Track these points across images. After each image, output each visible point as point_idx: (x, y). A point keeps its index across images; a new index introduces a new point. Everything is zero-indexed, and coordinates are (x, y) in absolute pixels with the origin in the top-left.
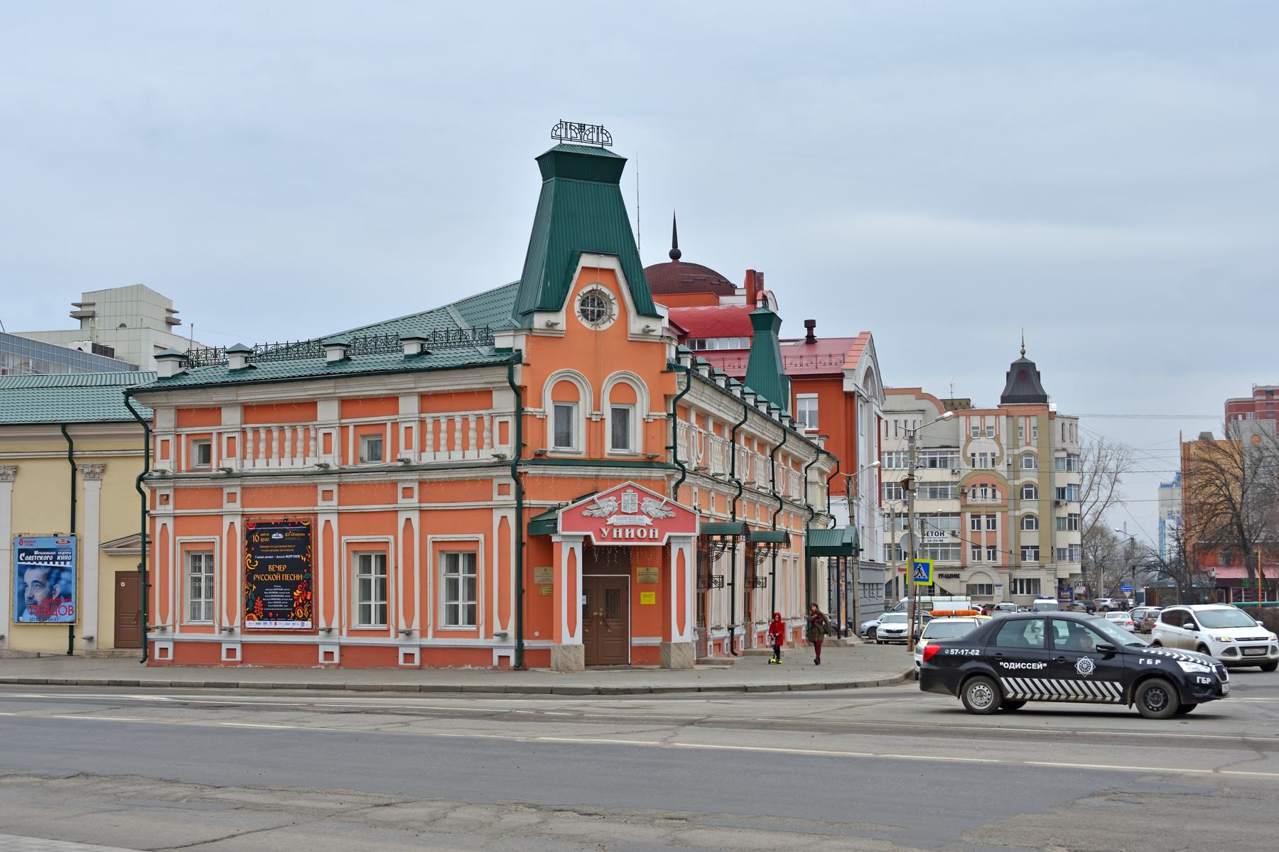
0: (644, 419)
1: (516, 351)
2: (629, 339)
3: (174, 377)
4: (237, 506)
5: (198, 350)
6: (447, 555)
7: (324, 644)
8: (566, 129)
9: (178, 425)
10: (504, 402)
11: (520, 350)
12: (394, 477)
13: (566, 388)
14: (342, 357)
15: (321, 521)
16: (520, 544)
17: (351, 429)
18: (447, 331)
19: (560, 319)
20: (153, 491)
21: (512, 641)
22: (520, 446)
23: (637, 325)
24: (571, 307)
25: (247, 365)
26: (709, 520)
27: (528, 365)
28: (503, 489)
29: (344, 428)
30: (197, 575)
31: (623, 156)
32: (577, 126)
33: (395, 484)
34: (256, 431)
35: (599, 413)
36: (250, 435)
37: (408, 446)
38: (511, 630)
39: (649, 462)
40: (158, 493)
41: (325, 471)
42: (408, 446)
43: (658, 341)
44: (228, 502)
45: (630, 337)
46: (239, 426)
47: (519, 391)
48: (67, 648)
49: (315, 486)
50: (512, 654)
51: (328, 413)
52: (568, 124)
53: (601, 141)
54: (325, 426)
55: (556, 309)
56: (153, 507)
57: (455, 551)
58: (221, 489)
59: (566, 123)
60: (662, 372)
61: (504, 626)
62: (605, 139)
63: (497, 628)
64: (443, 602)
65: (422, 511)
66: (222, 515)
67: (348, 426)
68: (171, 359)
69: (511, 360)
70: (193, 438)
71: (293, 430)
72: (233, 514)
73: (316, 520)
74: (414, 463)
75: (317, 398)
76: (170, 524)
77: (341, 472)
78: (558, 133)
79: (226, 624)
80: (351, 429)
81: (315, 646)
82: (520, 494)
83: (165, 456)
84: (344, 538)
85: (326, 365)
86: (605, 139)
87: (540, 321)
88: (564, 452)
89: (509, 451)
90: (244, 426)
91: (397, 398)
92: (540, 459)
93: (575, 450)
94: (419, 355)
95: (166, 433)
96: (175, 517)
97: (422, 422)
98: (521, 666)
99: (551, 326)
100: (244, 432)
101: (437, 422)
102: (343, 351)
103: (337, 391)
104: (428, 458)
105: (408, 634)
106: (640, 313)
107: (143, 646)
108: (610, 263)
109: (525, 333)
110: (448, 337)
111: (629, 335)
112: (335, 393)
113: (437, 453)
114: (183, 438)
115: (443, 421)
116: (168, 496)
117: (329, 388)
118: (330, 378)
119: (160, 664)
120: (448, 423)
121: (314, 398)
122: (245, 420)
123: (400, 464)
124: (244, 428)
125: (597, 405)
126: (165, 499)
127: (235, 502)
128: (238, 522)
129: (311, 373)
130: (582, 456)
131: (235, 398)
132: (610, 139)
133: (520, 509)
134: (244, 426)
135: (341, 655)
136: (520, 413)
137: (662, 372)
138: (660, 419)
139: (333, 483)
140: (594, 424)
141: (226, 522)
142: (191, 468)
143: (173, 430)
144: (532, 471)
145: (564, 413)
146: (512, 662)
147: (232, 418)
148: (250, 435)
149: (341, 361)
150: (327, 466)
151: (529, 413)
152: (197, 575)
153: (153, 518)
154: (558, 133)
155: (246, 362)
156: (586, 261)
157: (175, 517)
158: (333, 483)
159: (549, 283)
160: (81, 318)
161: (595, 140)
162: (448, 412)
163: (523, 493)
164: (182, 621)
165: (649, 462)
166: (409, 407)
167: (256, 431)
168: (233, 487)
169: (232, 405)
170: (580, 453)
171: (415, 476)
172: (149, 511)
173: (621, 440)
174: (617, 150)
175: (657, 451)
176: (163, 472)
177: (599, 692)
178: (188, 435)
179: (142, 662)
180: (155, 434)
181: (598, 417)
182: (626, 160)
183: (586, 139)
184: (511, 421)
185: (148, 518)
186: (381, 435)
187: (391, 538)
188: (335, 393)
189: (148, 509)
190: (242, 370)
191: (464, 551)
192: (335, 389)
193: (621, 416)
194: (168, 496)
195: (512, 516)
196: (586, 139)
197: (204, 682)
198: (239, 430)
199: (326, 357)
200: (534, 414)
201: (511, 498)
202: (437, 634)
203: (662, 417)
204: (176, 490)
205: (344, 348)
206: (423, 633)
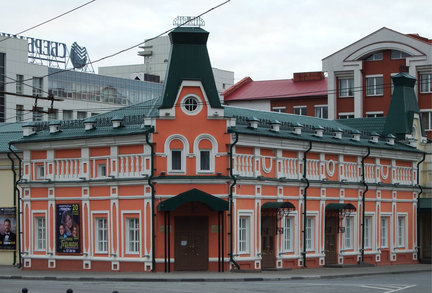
0: (216, 156)
1: (153, 126)
2: (208, 119)
3: (30, 136)
4: (116, 195)
5: (108, 118)
6: (130, 220)
7: (50, 259)
8: (181, 20)
9: (32, 158)
10: (147, 150)
11: (154, 126)
12: (109, 184)
13: (176, 142)
14: (92, 128)
15: (83, 203)
16: (154, 215)
17: (94, 161)
18: (130, 116)
19: (172, 112)
20: (23, 189)
21: (151, 259)
22: (153, 170)
23: (211, 112)
24: (178, 105)
25: (58, 130)
26: (339, 202)
27: (157, 133)
28: (148, 191)
29: (91, 161)
30: (40, 228)
31: (208, 31)
32: (186, 18)
33: (109, 187)
34: (60, 162)
35: (192, 154)
36: (58, 164)
37: (114, 170)
38: (151, 254)
39: (218, 176)
40: (25, 190)
41: (84, 181)
42: (114, 170)
43: (223, 119)
44: (147, 192)
45: (208, 118)
46: (117, 156)
47: (153, 145)
48: (13, 262)
49: (81, 188)
50: (151, 265)
51: (85, 154)
52: (182, 18)
53: (199, 24)
54: (146, 156)
55: (170, 107)
56: (23, 196)
57: (132, 218)
58: (47, 188)
59: (181, 17)
60: (225, 133)
61: (149, 253)
62: (201, 23)
63: (146, 254)
64: (128, 241)
65: (120, 200)
66: (48, 200)
67: (93, 160)
68: (28, 127)
69: (150, 129)
70: (38, 164)
71: (134, 157)
72: (51, 200)
73: (81, 203)
74: (116, 177)
75: (81, 147)
76: (29, 204)
77: (30, 183)
78: (177, 22)
79: (113, 252)
80: (94, 161)
81: (82, 261)
82: (154, 192)
83: (27, 173)
84: (123, 212)
85: (85, 131)
86: (201, 23)
87: (162, 113)
88: (177, 172)
89: (149, 172)
90: (55, 159)
91: (110, 147)
92: (163, 176)
93: (182, 171)
94: (118, 128)
95: (27, 162)
96: (90, 200)
97: (119, 159)
98: (154, 270)
99: (167, 114)
100: (55, 162)
101: (125, 158)
102: (120, 123)
103: (87, 144)
104: (121, 176)
105: (115, 256)
106: (213, 106)
107: (224, 264)
108: (198, 84)
109: (155, 118)
110: (139, 118)
111: (208, 117)
112: (86, 145)
113: (130, 172)
114: (34, 164)
115: (137, 157)
116: (28, 191)
117: (112, 141)
118: (82, 139)
119: (24, 269)
120: (124, 159)
121: (80, 147)
122: (119, 154)
123: (111, 178)
124: (56, 160)
125: (191, 150)
126: (27, 193)
127: (150, 192)
128: (54, 203)
129: (76, 136)
130: (185, 174)
131: (50, 147)
132: (203, 23)
133: (153, 198)
134: (55, 159)
135: (92, 265)
136: (153, 154)
137: (225, 133)
138: (224, 156)
139: (87, 186)
140: (191, 160)
141: (112, 202)
142: (37, 179)
143: (29, 161)
144: (158, 182)
145: (176, 156)
146: (151, 268)
147: (50, 156)
148: (58, 164)
149: (91, 130)
150: (85, 179)
151: (157, 155)
152: (40, 228)
153: (23, 202)
154: (177, 22)
155: (57, 129)
156: (185, 83)
157: (31, 201)
158: (87, 186)
159: (167, 95)
160: (145, 56)
161: (196, 24)
162: (75, 158)
163: (155, 192)
164: (34, 249)
165: (218, 176)
166: (114, 151)
167: (60, 162)
168: (51, 188)
169: (50, 149)
170: (183, 173)
171: (115, 184)
172: (21, 198)
173: (205, 164)
174: (205, 28)
175: (223, 172)
176: (26, 180)
177: (34, 279)
178: (36, 163)
179: (19, 268)
180: (23, 162)
181: (192, 156)
182: (209, 33)
183: (191, 24)
184: (150, 158)
185: (21, 202)
186: (105, 164)
187: (139, 212)
188: (86, 145)
189: (21, 197)
190: (56, 133)
191: (130, 218)
192: (86, 143)
193: (205, 156)
194: (28, 191)
195: (150, 201)
196: (191, 24)
197: (10, 276)
198: (53, 161)
199: (113, 126)
200: (160, 155)
201: (150, 194)
202: (126, 256)
203: (224, 155)
204: (90, 187)
205: (93, 124)
206: (120, 256)
